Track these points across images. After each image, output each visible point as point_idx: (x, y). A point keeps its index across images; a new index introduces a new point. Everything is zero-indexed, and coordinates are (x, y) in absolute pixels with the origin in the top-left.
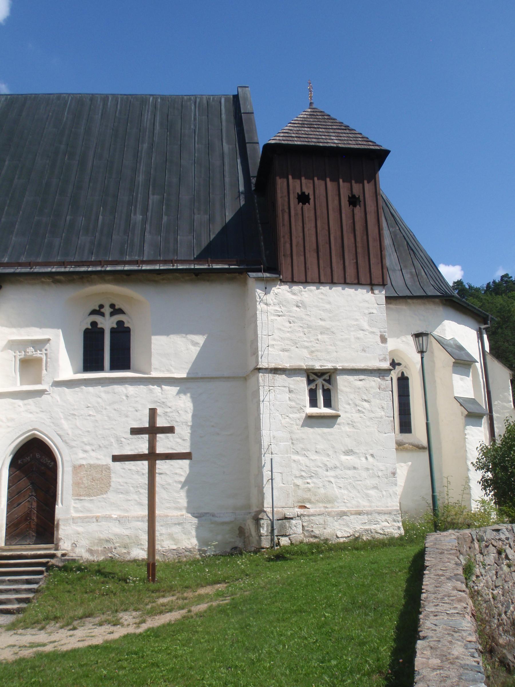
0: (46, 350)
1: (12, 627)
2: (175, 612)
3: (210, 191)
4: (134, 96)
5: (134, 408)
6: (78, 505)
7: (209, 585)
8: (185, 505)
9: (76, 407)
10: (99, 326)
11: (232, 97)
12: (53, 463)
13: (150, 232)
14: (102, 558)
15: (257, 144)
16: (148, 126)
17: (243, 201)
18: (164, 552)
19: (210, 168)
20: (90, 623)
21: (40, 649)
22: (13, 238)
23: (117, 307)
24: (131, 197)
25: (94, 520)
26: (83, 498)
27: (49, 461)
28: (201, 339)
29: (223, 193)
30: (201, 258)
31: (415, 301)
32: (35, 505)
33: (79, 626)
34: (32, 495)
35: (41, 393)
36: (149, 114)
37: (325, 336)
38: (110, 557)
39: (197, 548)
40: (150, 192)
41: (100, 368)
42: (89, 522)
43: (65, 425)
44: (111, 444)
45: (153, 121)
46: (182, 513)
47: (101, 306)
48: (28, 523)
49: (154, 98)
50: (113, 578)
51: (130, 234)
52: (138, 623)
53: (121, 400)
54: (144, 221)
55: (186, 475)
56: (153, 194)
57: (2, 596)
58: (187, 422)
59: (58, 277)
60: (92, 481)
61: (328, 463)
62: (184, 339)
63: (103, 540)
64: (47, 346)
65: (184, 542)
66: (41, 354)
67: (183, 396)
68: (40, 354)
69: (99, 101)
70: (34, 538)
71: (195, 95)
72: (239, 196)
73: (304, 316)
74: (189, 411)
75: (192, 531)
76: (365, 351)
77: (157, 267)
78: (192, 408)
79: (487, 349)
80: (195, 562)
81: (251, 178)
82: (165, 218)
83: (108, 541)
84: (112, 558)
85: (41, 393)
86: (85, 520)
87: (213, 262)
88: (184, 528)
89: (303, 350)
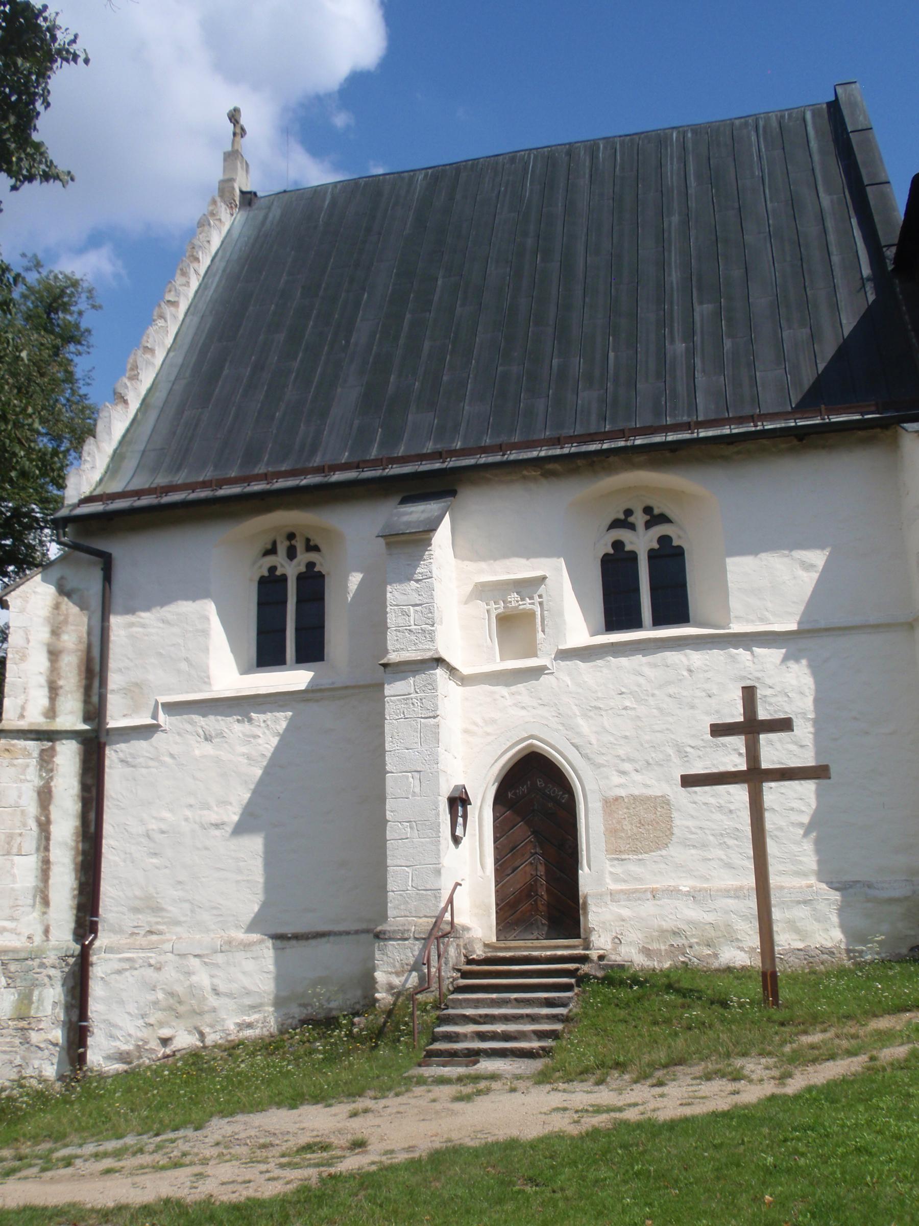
0: (540, 596)
1: (543, 1078)
2: (841, 1059)
3: (806, 284)
4: (643, 136)
5: (704, 691)
6: (618, 870)
7: (889, 1014)
8: (815, 867)
9: (600, 695)
10: (628, 548)
11: (825, 106)
12: (567, 796)
13: (704, 371)
14: (667, 965)
15: (887, 185)
16: (675, 184)
17: (872, 294)
18: (781, 954)
19: (801, 241)
20: (685, 1074)
21: (617, 1115)
22: (466, 408)
24: (662, 313)
25: (649, 896)
26: (627, 857)
27: (561, 793)
28: (818, 558)
29: (832, 284)
30: (807, 404)
32: (541, 870)
33: (668, 1080)
34: (536, 853)
35: (538, 672)
36: (675, 163)
38: (683, 962)
39: (843, 946)
40: (695, 300)
41: (635, 623)
42: (639, 899)
43: (584, 726)
44: (668, 759)
45: (682, 173)
46: (808, 882)
47: (629, 512)
48: (532, 901)
49: (679, 132)
50: (699, 998)
51: (668, 378)
52: (778, 1077)
53: (680, 678)
54: (691, 353)
55: (812, 812)
56: (701, 303)
57: (509, 1026)
58: (805, 714)
59: (551, 466)
60: (638, 825)
62: (786, 560)
63: (667, 931)
64: (542, 590)
65: (817, 935)
66: (533, 604)
67: (792, 664)
68: (530, 604)
69: (582, 153)
70: (546, 928)
71: (755, 115)
72: (864, 286)
74: (807, 692)
75: (831, 916)
77: (726, 431)
78: (813, 686)
80: (842, 972)
81: (884, 249)
82: (728, 344)
83: (676, 933)
84: (687, 965)
85: (538, 672)
86: (632, 896)
87: (830, 412)
88: (815, 910)
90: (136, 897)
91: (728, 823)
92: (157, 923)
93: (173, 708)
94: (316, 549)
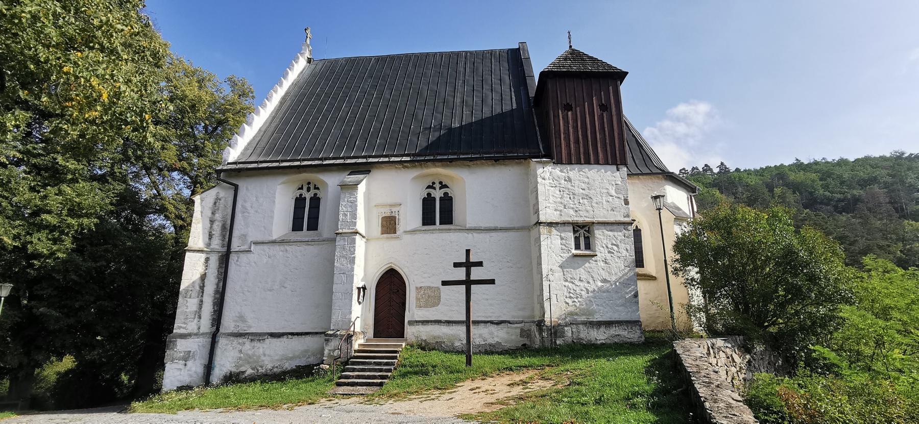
23: (443, 184)
31: (645, 177)
37: (585, 200)
47: (434, 183)
59: (406, 164)
61: (589, 288)
73: (570, 187)
76: (613, 211)
79: (695, 210)
89: (570, 210)
90: (236, 317)
91: (474, 295)
92: (244, 327)
93: (256, 243)
94: (318, 189)
